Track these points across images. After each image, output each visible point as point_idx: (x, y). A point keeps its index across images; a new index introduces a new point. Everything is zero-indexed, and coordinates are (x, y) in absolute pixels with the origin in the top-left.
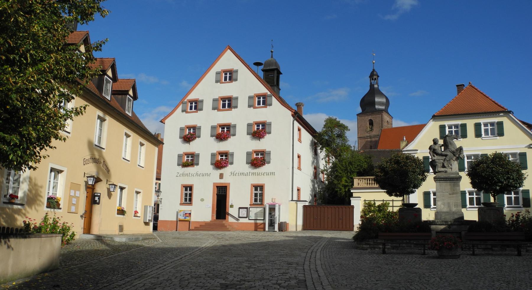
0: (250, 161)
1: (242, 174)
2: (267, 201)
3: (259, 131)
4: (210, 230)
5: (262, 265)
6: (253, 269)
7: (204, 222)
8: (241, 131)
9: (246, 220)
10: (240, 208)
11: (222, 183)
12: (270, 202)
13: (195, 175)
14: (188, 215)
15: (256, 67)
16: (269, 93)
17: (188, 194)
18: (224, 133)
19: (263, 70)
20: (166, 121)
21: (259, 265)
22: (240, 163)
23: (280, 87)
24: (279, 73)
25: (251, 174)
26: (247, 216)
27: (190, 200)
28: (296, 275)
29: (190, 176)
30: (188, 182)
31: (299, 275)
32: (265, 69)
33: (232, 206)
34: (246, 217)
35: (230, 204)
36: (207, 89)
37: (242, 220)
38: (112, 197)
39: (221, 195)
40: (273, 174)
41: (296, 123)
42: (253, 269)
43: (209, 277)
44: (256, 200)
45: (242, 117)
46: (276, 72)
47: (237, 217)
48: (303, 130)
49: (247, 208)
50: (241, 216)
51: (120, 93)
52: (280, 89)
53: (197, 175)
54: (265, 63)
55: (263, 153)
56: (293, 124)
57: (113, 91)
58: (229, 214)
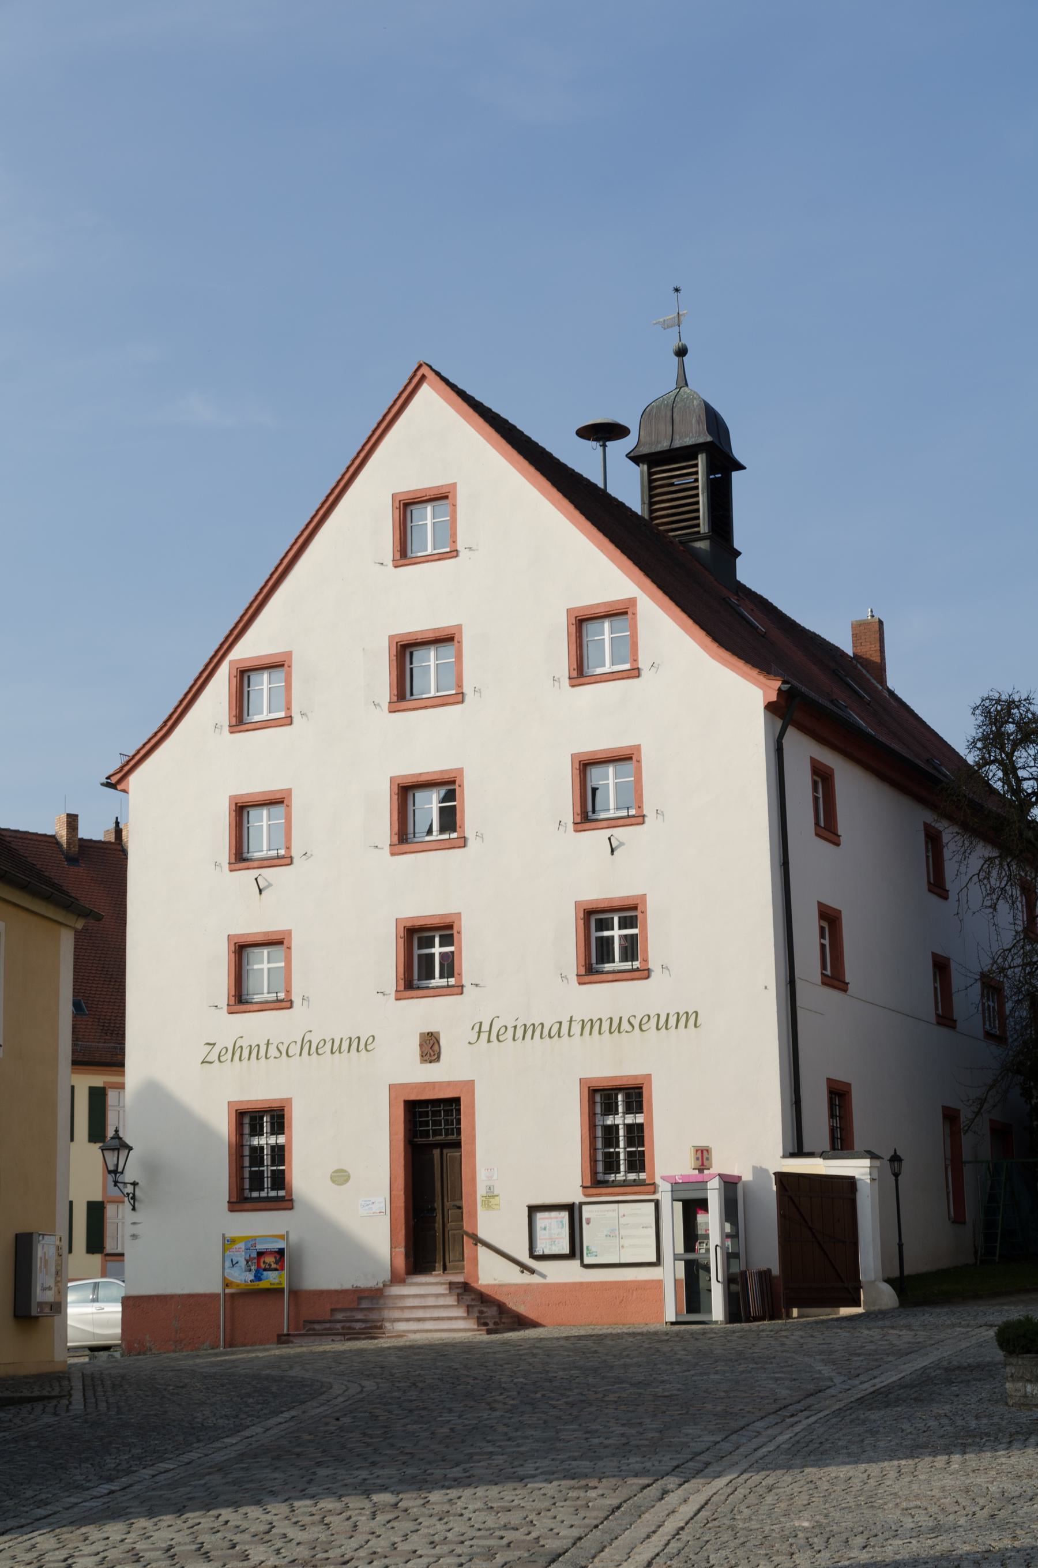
1: (530, 1030)
2: (669, 1159)
9: (569, 1272)
10: (533, 1210)
11: (433, 1085)
13: (295, 1050)
14: (270, 1259)
15: (592, 447)
19: (636, 459)
23: (737, 545)
25: (576, 1028)
26: (575, 1250)
32: (644, 450)
34: (571, 1255)
35: (481, 1191)
36: (341, 602)
39: (431, 1133)
40: (689, 1019)
47: (524, 1257)
49: (572, 1210)
50: (541, 1248)
51: (266, 863)
53: (308, 1047)
57: (833, 1147)
58: (477, 1240)
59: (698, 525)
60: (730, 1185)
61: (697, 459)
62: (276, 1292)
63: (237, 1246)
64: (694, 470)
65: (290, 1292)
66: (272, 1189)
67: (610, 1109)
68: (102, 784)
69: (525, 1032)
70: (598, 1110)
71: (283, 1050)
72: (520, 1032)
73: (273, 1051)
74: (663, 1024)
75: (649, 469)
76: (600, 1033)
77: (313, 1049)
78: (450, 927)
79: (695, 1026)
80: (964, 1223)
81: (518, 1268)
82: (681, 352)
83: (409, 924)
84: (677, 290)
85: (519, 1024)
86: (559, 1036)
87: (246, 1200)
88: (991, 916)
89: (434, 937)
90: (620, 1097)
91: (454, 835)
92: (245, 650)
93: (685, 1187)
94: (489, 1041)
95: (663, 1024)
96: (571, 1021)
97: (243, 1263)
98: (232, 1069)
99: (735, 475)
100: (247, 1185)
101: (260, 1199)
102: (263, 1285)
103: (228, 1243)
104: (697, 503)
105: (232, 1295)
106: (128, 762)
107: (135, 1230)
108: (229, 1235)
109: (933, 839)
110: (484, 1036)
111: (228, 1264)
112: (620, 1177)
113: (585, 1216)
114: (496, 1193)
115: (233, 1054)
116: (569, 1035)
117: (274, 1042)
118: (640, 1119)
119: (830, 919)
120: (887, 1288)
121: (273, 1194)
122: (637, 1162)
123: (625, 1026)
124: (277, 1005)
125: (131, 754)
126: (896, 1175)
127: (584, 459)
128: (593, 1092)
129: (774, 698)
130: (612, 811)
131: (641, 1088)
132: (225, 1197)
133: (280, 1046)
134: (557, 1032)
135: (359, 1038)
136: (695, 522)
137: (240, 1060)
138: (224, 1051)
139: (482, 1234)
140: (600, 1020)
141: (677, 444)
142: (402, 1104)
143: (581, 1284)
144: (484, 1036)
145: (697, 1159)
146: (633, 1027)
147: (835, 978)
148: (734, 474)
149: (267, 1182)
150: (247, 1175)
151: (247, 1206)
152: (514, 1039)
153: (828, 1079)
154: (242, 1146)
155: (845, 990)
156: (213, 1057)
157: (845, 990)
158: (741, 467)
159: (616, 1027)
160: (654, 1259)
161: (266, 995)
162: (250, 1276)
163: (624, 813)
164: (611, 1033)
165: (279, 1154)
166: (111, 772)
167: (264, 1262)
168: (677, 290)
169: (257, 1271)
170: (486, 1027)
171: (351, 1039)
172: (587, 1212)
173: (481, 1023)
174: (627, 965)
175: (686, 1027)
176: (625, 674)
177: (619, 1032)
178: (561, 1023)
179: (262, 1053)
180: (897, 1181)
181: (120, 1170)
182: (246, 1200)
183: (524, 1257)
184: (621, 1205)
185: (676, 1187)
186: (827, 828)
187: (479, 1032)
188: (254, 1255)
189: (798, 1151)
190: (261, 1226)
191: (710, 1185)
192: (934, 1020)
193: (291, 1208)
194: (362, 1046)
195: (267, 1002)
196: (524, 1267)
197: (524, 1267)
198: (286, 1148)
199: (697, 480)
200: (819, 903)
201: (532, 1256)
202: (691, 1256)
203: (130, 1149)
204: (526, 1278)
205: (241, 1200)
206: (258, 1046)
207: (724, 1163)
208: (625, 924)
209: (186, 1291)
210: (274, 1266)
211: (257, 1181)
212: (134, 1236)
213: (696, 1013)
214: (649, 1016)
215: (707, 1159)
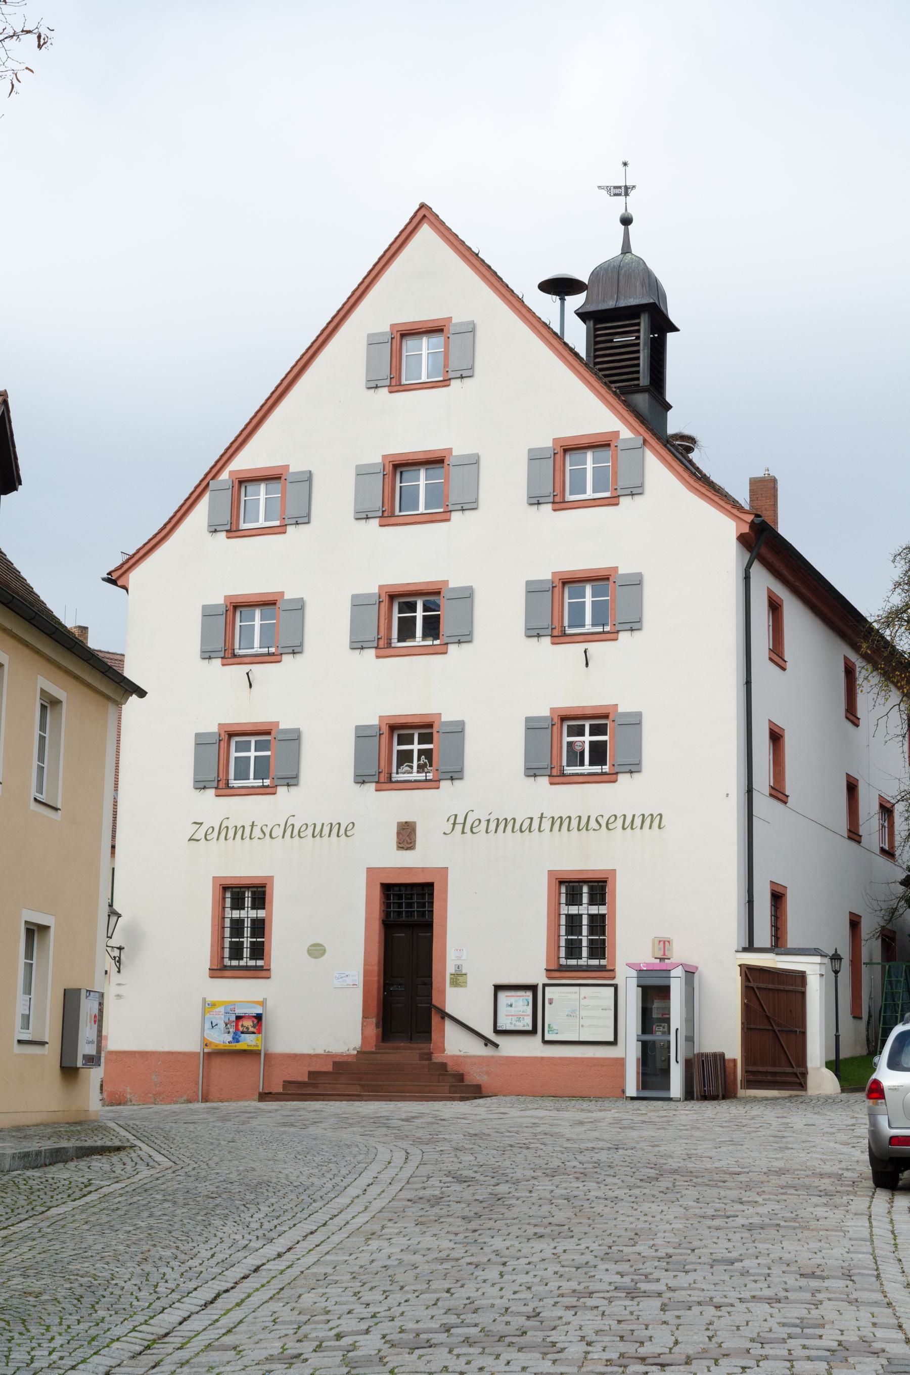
1: (504, 824)
2: (631, 949)
4: (358, 1097)
5: (684, 1280)
6: (657, 1303)
7: (328, 1056)
8: (499, 613)
9: (530, 1048)
10: (498, 988)
12: (646, 957)
13: (278, 832)
14: (248, 1023)
15: (552, 301)
16: (626, 433)
17: (243, 924)
19: (583, 315)
20: (134, 578)
21: (673, 1283)
23: (669, 398)
24: (662, 325)
25: (546, 824)
27: (258, 951)
28: (867, 1332)
29: (257, 836)
30: (244, 866)
31: (880, 1333)
32: (591, 308)
33: (459, 979)
34: (534, 1031)
35: (450, 969)
37: (511, 1048)
39: (407, 915)
40: (654, 821)
41: (760, 575)
42: (657, 1303)
43: (468, 1341)
44: (573, 950)
45: (497, 551)
46: (644, 322)
48: (795, 614)
49: (533, 988)
50: (504, 1024)
52: (668, 407)
54: (595, 275)
56: (747, 578)
58: (444, 1015)
59: (638, 379)
61: (639, 317)
62: (252, 1054)
63: (217, 1010)
64: (636, 328)
65: (265, 1054)
66: (251, 959)
67: (574, 898)
68: (104, 579)
69: (497, 826)
70: (563, 900)
71: (603, 822)
72: (492, 826)
73: (257, 833)
74: (628, 824)
75: (595, 324)
76: (569, 830)
77: (296, 832)
78: (430, 726)
79: (659, 827)
80: (861, 1018)
81: (482, 1042)
82: (626, 221)
83: (392, 722)
84: (625, 164)
85: (492, 818)
86: (530, 831)
87: (225, 968)
88: (900, 744)
89: (413, 734)
90: (585, 889)
91: (437, 642)
92: (243, 462)
94: (463, 832)
95: (628, 824)
96: (541, 818)
98: (215, 847)
99: (670, 336)
101: (239, 968)
103: (208, 1006)
104: (638, 358)
106: (128, 560)
107: (120, 991)
108: (210, 999)
109: (850, 672)
110: (459, 828)
111: (208, 1025)
112: (583, 962)
114: (464, 972)
115: (219, 833)
116: (540, 831)
117: (259, 824)
118: (603, 910)
120: (829, 1075)
121: (252, 963)
122: (598, 949)
123: (593, 824)
124: (262, 791)
125: (131, 553)
126: (836, 972)
128: (225, 888)
129: (746, 529)
130: (587, 627)
131: (606, 882)
132: (207, 965)
133: (264, 828)
134: (528, 827)
135: (339, 824)
136: (635, 376)
137: (226, 839)
138: (211, 830)
139: (448, 1010)
141: (622, 304)
142: (378, 887)
143: (542, 1058)
144: (459, 828)
145: (660, 949)
146: (600, 826)
148: (668, 334)
149: (246, 953)
150: (227, 945)
152: (487, 832)
154: (224, 918)
156: (200, 835)
158: (675, 329)
159: (584, 825)
160: (612, 1039)
161: (415, 774)
163: (600, 629)
164: (579, 830)
166: (112, 568)
167: (242, 1026)
168: (625, 164)
170: (460, 820)
171: (331, 824)
173: (456, 816)
174: (597, 769)
175: (650, 828)
176: (605, 502)
177: (587, 829)
178: (532, 819)
179: (247, 833)
180: (836, 977)
182: (225, 968)
183: (489, 1033)
184: (582, 988)
185: (643, 974)
187: (454, 824)
189: (750, 948)
190: (241, 992)
191: (673, 973)
194: (342, 831)
195: (253, 787)
196: (488, 1042)
197: (488, 1042)
198: (266, 922)
199: (638, 338)
201: (497, 1032)
202: (647, 1037)
203: (119, 916)
204: (488, 1052)
206: (243, 827)
208: (595, 730)
209: (166, 1049)
210: (251, 1029)
212: (118, 996)
213: (661, 815)
215: (669, 949)
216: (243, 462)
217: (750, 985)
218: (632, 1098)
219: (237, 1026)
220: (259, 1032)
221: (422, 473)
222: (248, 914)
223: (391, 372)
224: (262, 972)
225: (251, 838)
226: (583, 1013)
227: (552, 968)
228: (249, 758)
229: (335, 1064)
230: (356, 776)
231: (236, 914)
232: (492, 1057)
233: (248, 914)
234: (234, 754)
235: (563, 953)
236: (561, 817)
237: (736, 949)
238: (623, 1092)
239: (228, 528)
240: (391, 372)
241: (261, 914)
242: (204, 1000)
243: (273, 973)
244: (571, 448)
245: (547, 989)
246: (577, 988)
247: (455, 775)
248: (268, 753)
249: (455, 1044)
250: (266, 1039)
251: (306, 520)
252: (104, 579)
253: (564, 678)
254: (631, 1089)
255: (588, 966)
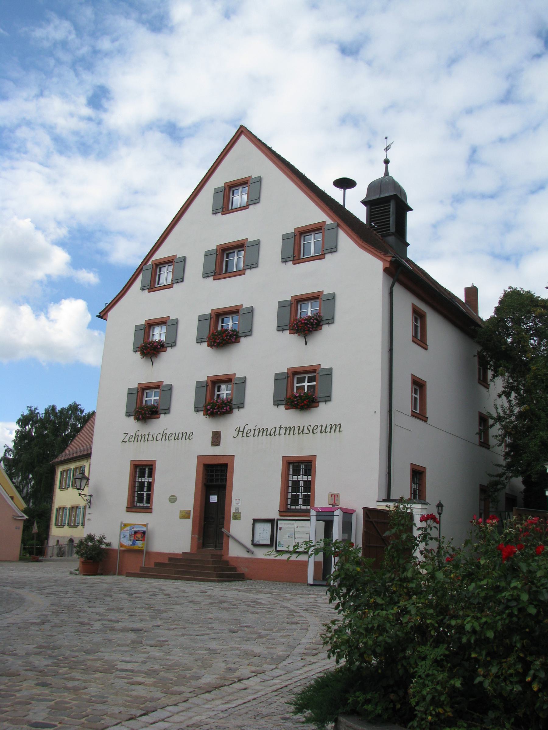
0: (283, 397)
1: (263, 431)
2: (321, 500)
3: (305, 319)
10: (255, 521)
13: (159, 437)
14: (139, 536)
16: (329, 221)
18: (222, 332)
22: (260, 405)
23: (408, 240)
25: (283, 431)
26: (273, 543)
30: (144, 456)
33: (237, 516)
34: (271, 545)
35: (233, 510)
38: (477, 418)
40: (337, 428)
44: (295, 501)
45: (266, 288)
47: (249, 544)
49: (271, 521)
50: (258, 540)
53: (165, 437)
55: (312, 373)
60: (348, 514)
62: (140, 551)
68: (97, 316)
70: (291, 473)
71: (311, 429)
73: (151, 438)
74: (323, 431)
77: (268, 433)
78: (314, 371)
79: (339, 432)
93: (324, 514)
94: (243, 436)
97: (128, 536)
98: (133, 446)
100: (289, 502)
101: (140, 507)
102: (135, 547)
105: (124, 551)
106: (108, 306)
108: (125, 522)
110: (241, 434)
111: (122, 536)
113: (279, 526)
119: (419, 385)
122: (308, 500)
123: (306, 431)
127: (336, 194)
128: (289, 463)
129: (388, 265)
131: (311, 462)
140: (294, 427)
142: (202, 466)
144: (241, 434)
145: (332, 499)
147: (420, 413)
149: (301, 501)
150: (290, 497)
151: (133, 510)
153: (411, 464)
155: (426, 421)
157: (426, 421)
158: (411, 209)
162: (130, 543)
165: (150, 486)
169: (134, 541)
170: (241, 430)
172: (281, 524)
178: (276, 428)
181: (82, 488)
185: (320, 514)
186: (420, 339)
187: (239, 432)
188: (133, 533)
190: (138, 519)
192: (478, 444)
193: (151, 512)
200: (412, 375)
205: (131, 508)
207: (345, 502)
210: (141, 539)
211: (295, 501)
212: (89, 520)
213: (340, 424)
214: (317, 426)
215: (337, 500)
216: (159, 255)
217: (369, 520)
218: (311, 585)
219: (134, 536)
220: (144, 540)
221: (313, 237)
222: (302, 478)
223: (224, 205)
224: (148, 510)
225: (279, 435)
226: (297, 536)
227: (282, 510)
228: (304, 386)
229: (170, 559)
230: (274, 401)
231: (295, 478)
232: (251, 558)
233: (302, 478)
234: (296, 385)
235: (289, 502)
236: (336, 425)
237: (377, 500)
238: (307, 581)
239: (149, 287)
240: (224, 205)
241: (310, 478)
242: (122, 523)
243: (154, 511)
244: (303, 232)
245: (279, 522)
246: (293, 522)
247: (240, 406)
248: (314, 383)
249: (234, 551)
250: (147, 544)
251: (181, 280)
252: (97, 316)
253: (293, 353)
254: (310, 580)
255: (301, 509)
